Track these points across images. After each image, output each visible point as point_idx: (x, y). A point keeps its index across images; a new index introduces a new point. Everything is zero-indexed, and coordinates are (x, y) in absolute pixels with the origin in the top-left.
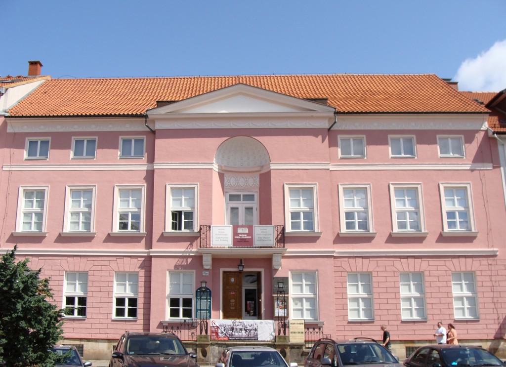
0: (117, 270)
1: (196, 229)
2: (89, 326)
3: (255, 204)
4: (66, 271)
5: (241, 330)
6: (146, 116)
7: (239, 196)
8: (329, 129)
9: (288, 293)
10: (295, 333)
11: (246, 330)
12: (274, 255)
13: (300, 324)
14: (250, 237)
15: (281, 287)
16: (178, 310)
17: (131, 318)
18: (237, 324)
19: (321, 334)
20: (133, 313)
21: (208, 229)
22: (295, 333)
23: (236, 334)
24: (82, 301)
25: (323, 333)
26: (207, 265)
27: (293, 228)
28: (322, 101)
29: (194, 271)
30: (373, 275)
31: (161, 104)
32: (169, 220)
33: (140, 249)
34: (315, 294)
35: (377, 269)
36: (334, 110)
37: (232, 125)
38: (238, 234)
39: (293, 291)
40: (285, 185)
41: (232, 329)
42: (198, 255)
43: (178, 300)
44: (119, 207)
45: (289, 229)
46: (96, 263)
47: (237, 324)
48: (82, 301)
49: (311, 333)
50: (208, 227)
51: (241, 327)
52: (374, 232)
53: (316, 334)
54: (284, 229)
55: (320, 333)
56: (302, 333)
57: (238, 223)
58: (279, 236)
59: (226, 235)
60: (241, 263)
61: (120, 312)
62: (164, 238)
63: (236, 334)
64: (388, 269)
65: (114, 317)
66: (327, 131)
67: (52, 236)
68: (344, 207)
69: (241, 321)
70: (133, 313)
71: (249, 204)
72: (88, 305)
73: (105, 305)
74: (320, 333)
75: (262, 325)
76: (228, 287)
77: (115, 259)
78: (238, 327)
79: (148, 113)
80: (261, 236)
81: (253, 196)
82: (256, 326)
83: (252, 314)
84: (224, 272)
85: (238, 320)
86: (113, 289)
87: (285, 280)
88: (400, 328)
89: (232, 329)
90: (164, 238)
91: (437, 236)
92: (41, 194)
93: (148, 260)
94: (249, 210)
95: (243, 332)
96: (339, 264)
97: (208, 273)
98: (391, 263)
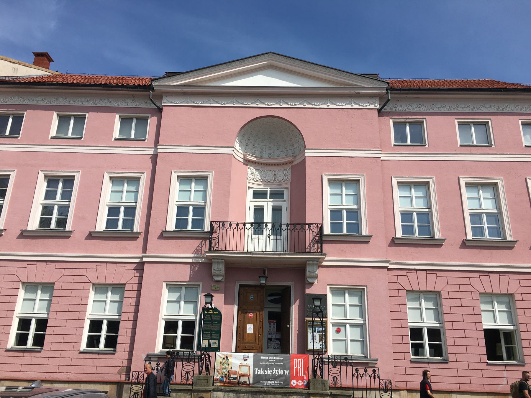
0: (95, 281)
1: (207, 228)
2: (44, 361)
3: (285, 205)
4: (93, 284)
6: (150, 88)
12: (308, 262)
15: (316, 309)
16: (422, 346)
19: (377, 379)
20: (111, 342)
21: (221, 226)
24: (42, 324)
25: (379, 377)
26: (218, 276)
27: (474, 234)
28: (373, 76)
29: (201, 284)
30: (443, 297)
31: (170, 75)
33: (131, 252)
34: (364, 320)
35: (448, 288)
36: (386, 85)
39: (333, 315)
40: (324, 175)
42: (207, 261)
43: (175, 323)
44: (108, 196)
45: (327, 231)
46: (450, 281)
48: (42, 324)
49: (370, 377)
50: (221, 224)
52: (513, 240)
53: (360, 378)
54: (321, 229)
55: (374, 376)
58: (317, 238)
60: (264, 273)
61: (93, 341)
62: (164, 235)
64: (463, 288)
65: (83, 346)
67: (80, 235)
68: (469, 207)
70: (111, 342)
72: (49, 330)
73: (72, 331)
74: (374, 376)
77: (477, 275)
79: (154, 84)
83: (214, 344)
84: (241, 286)
86: (86, 308)
87: (323, 298)
88: (485, 374)
90: (164, 235)
91: (460, 242)
92: (69, 181)
93: (140, 267)
96: (394, 279)
98: (467, 281)
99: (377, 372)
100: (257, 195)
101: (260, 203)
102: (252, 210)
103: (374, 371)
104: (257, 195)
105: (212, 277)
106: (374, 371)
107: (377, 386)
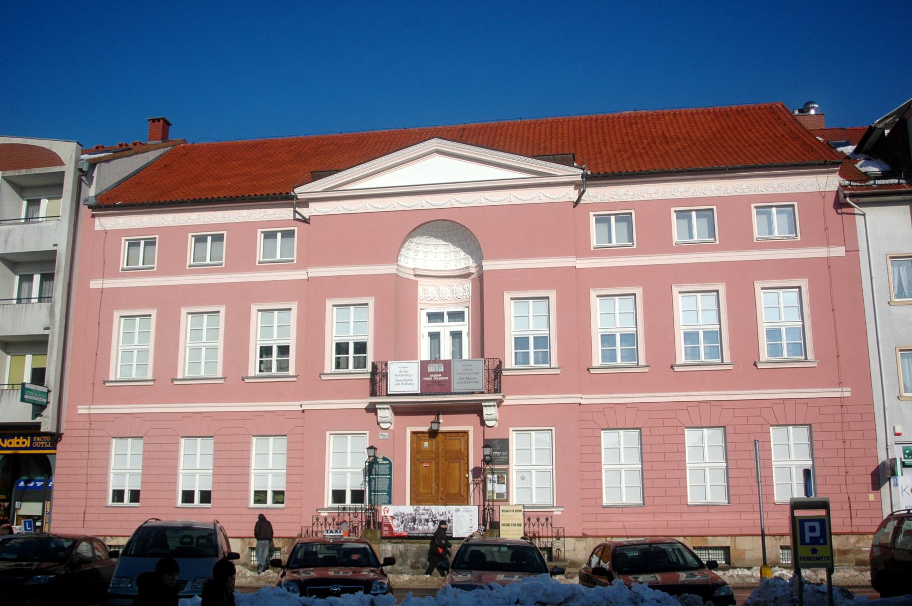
3: (464, 327)
5: (427, 521)
7: (442, 314)
8: (576, 203)
9: (507, 462)
10: (508, 525)
11: (434, 522)
13: (517, 511)
14: (446, 378)
15: (497, 451)
17: (336, 505)
18: (421, 512)
19: (550, 527)
22: (508, 525)
23: (420, 528)
32: (330, 355)
37: (483, 200)
38: (428, 374)
41: (414, 520)
45: (509, 362)
47: (421, 512)
51: (426, 517)
56: (520, 525)
57: (176, 374)
59: (410, 376)
63: (420, 528)
66: (572, 205)
69: (427, 507)
71: (457, 326)
75: (459, 514)
76: (419, 456)
78: (422, 517)
80: (464, 376)
81: (462, 313)
82: (449, 515)
84: (413, 433)
85: (422, 507)
89: (414, 520)
94: (456, 335)
95: (431, 524)
97: (387, 434)
99: (550, 520)
100: (434, 317)
101: (435, 327)
102: (426, 335)
103: (547, 519)
104: (434, 317)
105: (378, 424)
106: (547, 519)
107: (550, 534)
